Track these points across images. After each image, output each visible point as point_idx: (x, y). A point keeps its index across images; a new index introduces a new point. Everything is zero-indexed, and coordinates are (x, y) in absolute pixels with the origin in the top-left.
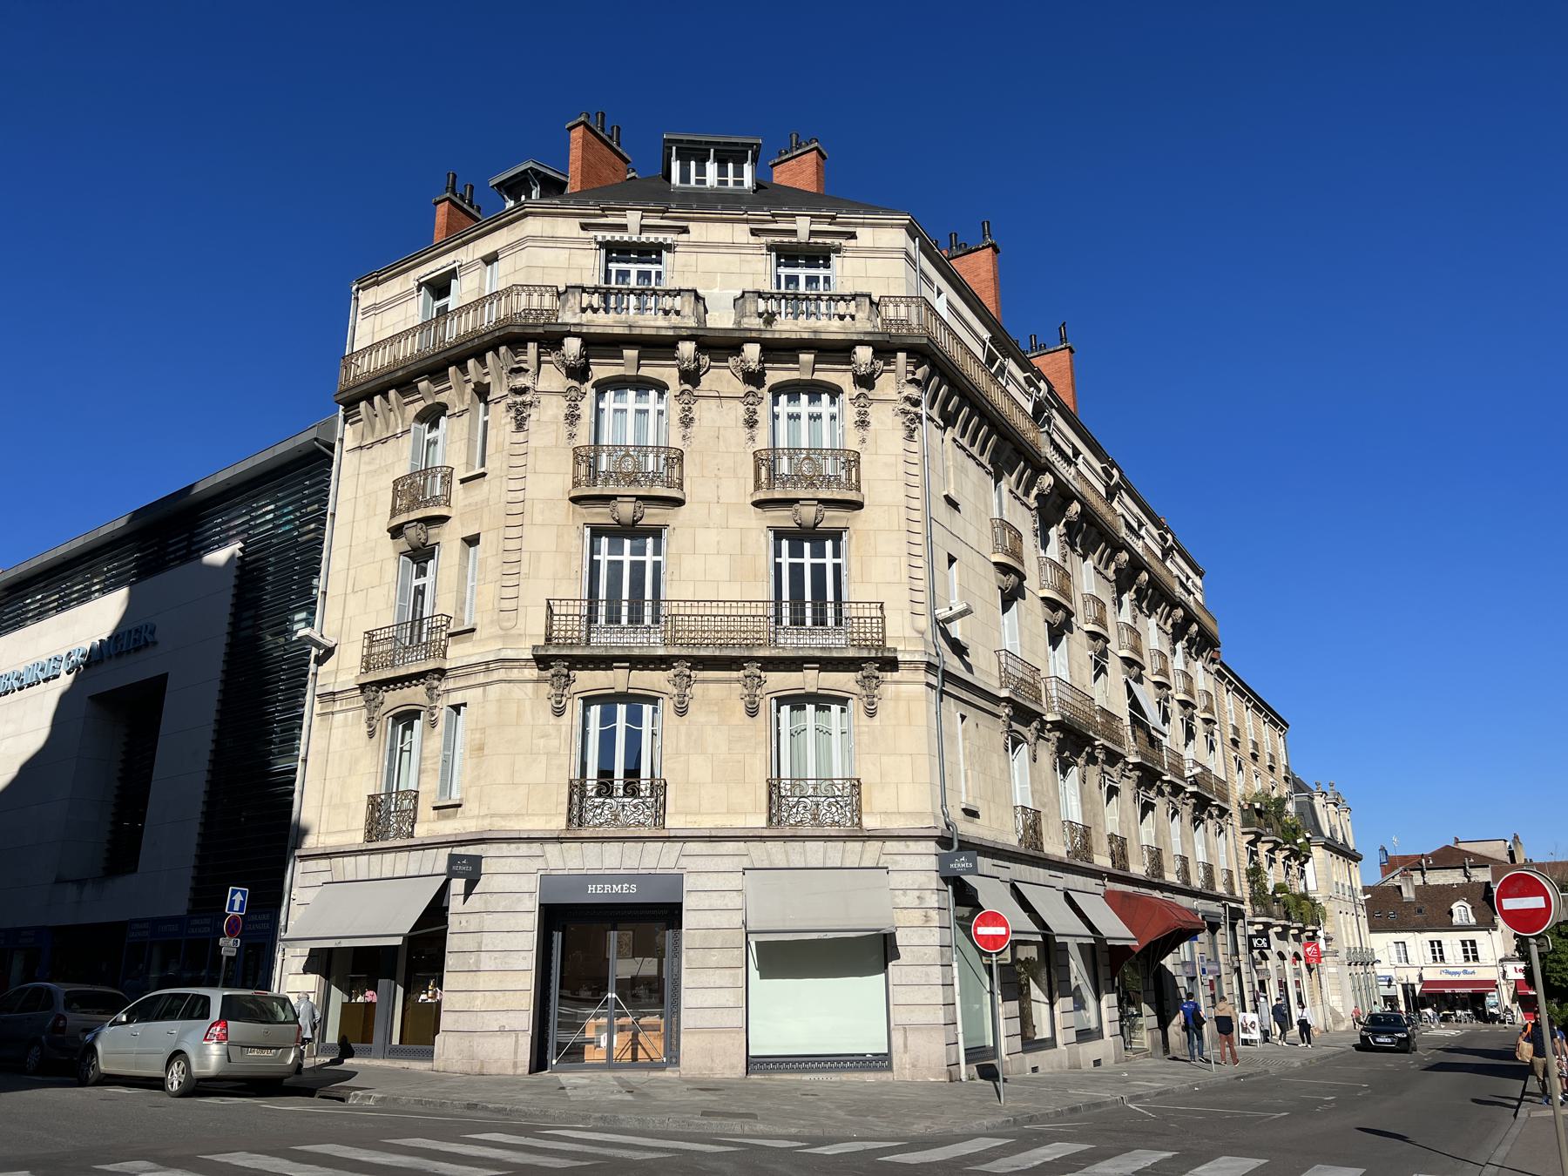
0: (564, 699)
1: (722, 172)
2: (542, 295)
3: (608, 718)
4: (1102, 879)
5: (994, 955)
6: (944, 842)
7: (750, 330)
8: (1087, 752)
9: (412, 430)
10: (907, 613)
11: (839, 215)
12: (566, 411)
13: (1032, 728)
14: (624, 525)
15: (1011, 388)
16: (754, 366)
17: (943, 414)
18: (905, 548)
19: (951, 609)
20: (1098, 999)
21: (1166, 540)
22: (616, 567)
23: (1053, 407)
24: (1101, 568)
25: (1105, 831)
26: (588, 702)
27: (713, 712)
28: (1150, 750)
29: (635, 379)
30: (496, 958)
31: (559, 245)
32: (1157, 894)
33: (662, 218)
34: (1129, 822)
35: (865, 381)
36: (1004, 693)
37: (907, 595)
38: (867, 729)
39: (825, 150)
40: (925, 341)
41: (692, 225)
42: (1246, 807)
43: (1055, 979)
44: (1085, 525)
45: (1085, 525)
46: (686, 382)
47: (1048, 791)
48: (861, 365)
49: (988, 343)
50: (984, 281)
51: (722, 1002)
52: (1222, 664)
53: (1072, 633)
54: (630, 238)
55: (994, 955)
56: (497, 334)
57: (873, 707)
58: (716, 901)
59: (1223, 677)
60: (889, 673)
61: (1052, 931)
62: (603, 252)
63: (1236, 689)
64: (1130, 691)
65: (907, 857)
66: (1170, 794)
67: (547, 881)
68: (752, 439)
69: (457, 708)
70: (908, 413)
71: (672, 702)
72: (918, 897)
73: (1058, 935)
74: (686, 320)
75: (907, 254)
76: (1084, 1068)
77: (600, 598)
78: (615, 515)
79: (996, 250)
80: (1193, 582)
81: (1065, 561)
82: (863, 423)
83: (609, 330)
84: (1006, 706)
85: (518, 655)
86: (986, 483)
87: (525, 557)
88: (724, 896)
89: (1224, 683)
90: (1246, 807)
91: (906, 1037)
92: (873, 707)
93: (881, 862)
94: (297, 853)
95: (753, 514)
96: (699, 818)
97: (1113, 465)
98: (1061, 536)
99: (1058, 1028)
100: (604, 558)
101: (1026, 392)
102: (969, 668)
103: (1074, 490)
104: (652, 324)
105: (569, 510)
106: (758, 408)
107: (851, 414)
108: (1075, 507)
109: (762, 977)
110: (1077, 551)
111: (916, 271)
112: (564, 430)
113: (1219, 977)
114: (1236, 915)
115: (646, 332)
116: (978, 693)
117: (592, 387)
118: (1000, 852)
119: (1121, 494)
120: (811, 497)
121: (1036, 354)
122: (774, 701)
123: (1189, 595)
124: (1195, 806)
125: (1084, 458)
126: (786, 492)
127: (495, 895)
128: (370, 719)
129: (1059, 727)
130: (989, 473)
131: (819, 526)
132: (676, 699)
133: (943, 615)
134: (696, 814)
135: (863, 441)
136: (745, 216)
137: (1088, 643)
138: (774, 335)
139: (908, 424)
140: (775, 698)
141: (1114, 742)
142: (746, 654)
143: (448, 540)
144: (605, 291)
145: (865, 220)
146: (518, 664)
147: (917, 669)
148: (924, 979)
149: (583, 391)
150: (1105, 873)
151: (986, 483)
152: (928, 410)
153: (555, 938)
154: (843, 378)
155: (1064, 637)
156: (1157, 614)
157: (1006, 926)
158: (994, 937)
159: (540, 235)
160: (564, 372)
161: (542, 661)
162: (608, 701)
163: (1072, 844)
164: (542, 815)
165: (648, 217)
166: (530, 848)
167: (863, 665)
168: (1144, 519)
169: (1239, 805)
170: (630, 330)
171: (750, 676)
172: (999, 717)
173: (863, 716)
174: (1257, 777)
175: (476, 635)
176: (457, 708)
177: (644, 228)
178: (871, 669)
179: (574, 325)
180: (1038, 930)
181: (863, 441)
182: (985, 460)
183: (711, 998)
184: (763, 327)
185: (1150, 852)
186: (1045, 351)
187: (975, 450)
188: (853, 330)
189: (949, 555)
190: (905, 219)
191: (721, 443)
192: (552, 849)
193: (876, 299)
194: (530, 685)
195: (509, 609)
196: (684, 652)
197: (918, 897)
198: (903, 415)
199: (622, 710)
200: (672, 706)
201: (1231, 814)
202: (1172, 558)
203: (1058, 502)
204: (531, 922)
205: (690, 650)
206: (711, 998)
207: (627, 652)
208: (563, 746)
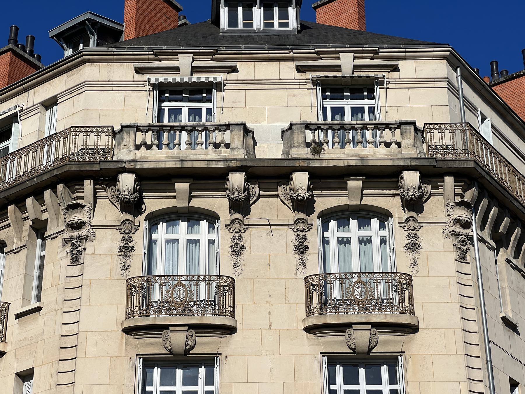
1: (268, 15)
7: (299, 159)
11: (381, 50)
14: (176, 355)
16: (303, 193)
18: (463, 373)
29: (187, 211)
33: (212, 60)
40: (472, 165)
46: (236, 212)
48: (409, 190)
56: (55, 173)
62: (156, 93)
68: (303, 265)
74: (235, 153)
75: (449, 83)
78: (168, 344)
83: (162, 165)
95: (305, 338)
104: (203, 157)
106: (308, 234)
111: (459, 98)
112: (118, 261)
120: (363, 321)
135: (415, 264)
136: (291, 55)
165: (199, 59)
170: (182, 164)
177: (194, 70)
179: (129, 161)
181: (415, 264)
184: (310, 156)
188: (399, 156)
190: (446, 51)
193: (421, 127)
198: (454, 237)
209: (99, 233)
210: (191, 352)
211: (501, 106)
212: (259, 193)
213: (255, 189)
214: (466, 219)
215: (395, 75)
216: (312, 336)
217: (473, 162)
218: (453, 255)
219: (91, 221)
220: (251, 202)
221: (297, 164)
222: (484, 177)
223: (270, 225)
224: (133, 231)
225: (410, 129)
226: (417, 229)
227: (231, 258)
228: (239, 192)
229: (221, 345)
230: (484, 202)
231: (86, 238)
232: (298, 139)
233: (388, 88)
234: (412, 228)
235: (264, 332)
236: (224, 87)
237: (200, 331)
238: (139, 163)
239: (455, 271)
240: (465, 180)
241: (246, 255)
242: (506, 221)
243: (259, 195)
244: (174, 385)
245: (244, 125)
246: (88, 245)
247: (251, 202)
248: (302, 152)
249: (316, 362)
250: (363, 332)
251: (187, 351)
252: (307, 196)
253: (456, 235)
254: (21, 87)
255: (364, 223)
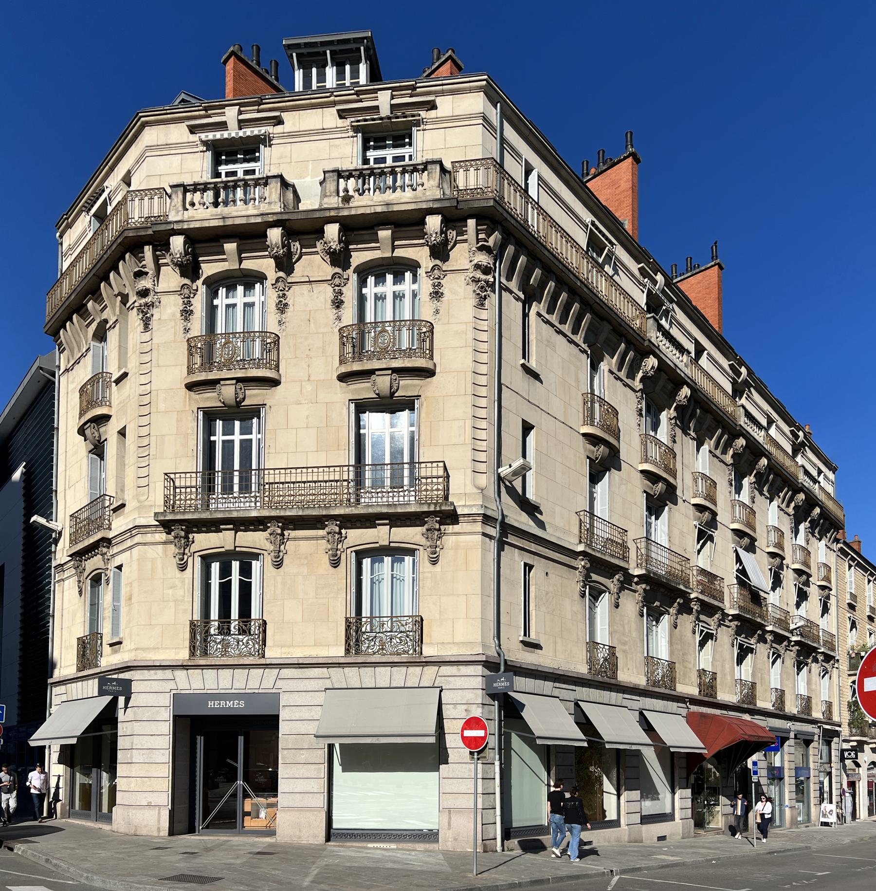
0: (186, 557)
1: (340, 75)
2: (152, 199)
3: (225, 571)
4: (685, 703)
5: (476, 754)
6: (490, 665)
7: (329, 209)
8: (679, 603)
9: (91, 348)
10: (469, 472)
11: (418, 85)
12: (181, 308)
13: (615, 580)
14: (230, 407)
15: (624, 280)
16: (335, 245)
17: (524, 285)
18: (469, 411)
19: (510, 466)
20: (673, 792)
21: (797, 437)
22: (228, 446)
23: (671, 301)
24: (718, 452)
25: (694, 665)
26: (207, 560)
27: (303, 564)
28: (751, 606)
29: (240, 274)
30: (143, 754)
31: (172, 152)
32: (747, 717)
33: (259, 111)
34: (724, 661)
35: (440, 252)
36: (581, 548)
37: (469, 455)
38: (429, 575)
39: (459, 59)
40: (491, 203)
41: (285, 116)
42: (853, 655)
43: (622, 777)
44: (698, 411)
45: (698, 411)
46: (280, 270)
47: (630, 631)
48: (431, 235)
49: (590, 226)
50: (623, 191)
51: (309, 789)
52: (845, 543)
53: (676, 504)
54: (230, 134)
55: (476, 754)
56: (119, 241)
57: (435, 556)
58: (305, 713)
59: (846, 554)
60: (451, 526)
61: (601, 738)
62: (209, 154)
63: (859, 565)
64: (738, 560)
65: (459, 678)
66: (772, 641)
67: (178, 698)
68: (339, 319)
69: (120, 567)
70: (479, 281)
71: (269, 557)
72: (466, 710)
73: (539, 738)
74: (272, 206)
75: (485, 119)
76: (647, 842)
77: (217, 470)
78: (221, 398)
79: (637, 160)
80: (825, 475)
81: (674, 442)
82: (437, 295)
83: (206, 224)
84: (583, 560)
85: (148, 522)
86: (580, 361)
87: (153, 440)
88: (311, 710)
89: (847, 560)
90: (853, 655)
91: (450, 818)
92: (435, 556)
93: (437, 682)
94: (50, 681)
95: (339, 387)
96: (291, 650)
97: (741, 363)
98: (671, 419)
99: (622, 813)
100: (218, 438)
101: (640, 283)
102: (541, 525)
103: (683, 375)
104: (244, 213)
105: (185, 397)
106: (344, 289)
107: (425, 285)
108: (685, 391)
109: (344, 771)
110: (689, 434)
111: (496, 138)
112: (180, 324)
113: (808, 778)
114: (829, 736)
115: (238, 221)
116: (551, 547)
117: (203, 284)
118: (562, 677)
119: (750, 391)
120: (384, 366)
121: (689, 274)
122: (354, 554)
123: (815, 483)
124: (799, 653)
125: (708, 354)
126: (363, 366)
127: (141, 709)
128: (79, 581)
129: (645, 580)
130: (584, 351)
131: (396, 395)
132: (272, 554)
133: (504, 472)
134: (289, 646)
135: (437, 312)
136: (332, 98)
137: (694, 513)
138: (350, 211)
139: (478, 292)
140: (355, 551)
141: (714, 598)
142: (324, 513)
143: (110, 431)
144: (203, 187)
145: (445, 87)
146: (150, 529)
147: (475, 521)
148: (467, 774)
149: (195, 288)
150: (687, 698)
151: (580, 361)
152: (503, 280)
153: (198, 741)
154: (420, 253)
155: (667, 508)
156: (779, 497)
157: (485, 729)
158: (475, 738)
159: (156, 144)
160: (178, 272)
161: (167, 525)
162: (225, 558)
163: (741, 694)
164: (173, 648)
165: (246, 112)
166: (165, 673)
167: (426, 519)
168: (775, 416)
169: (848, 654)
170: (224, 222)
171: (331, 533)
172: (576, 569)
173: (427, 564)
174: (871, 634)
175: (126, 508)
176: (120, 567)
177: (242, 124)
178: (433, 523)
179: (177, 222)
180: (651, 743)
181: (437, 312)
182: (579, 339)
183: (301, 785)
184: (341, 205)
185: (802, 699)
186: (697, 270)
187: (566, 328)
188: (424, 199)
189: (524, 421)
190: (481, 80)
191: (312, 325)
192: (180, 674)
193: (448, 165)
194: (160, 547)
195: (144, 484)
196: (274, 513)
197: (466, 710)
198: (474, 284)
199: (236, 565)
200: (270, 561)
201: (838, 661)
202: (803, 453)
203: (669, 387)
204: (167, 728)
205: (278, 511)
206: (301, 785)
207: (227, 515)
208: (186, 595)
209: (164, 299)
210: (242, 404)
211: (552, 157)
212: (301, 250)
213: (296, 246)
214: (485, 264)
215: (432, 114)
216: (344, 384)
217: (492, 200)
218: (472, 301)
219: (156, 287)
220: (294, 260)
221: (327, 214)
222: (506, 219)
223: (310, 282)
224: (192, 295)
225: (436, 169)
226: (442, 277)
227: (277, 316)
228: (278, 248)
229: (267, 397)
230: (510, 249)
231: (153, 305)
232: (330, 187)
233: (425, 130)
234: (436, 276)
235: (304, 383)
236: (270, 142)
237: (247, 384)
238: (186, 223)
239: (471, 317)
240: (487, 222)
241: (290, 311)
242: (537, 272)
243: (301, 253)
244: (233, 434)
245: (281, 177)
246: (155, 311)
247: (294, 260)
248: (333, 202)
249: (345, 408)
250: (384, 377)
251: (238, 404)
252: (338, 248)
253: (476, 281)
254: (107, 167)
255: (399, 278)
